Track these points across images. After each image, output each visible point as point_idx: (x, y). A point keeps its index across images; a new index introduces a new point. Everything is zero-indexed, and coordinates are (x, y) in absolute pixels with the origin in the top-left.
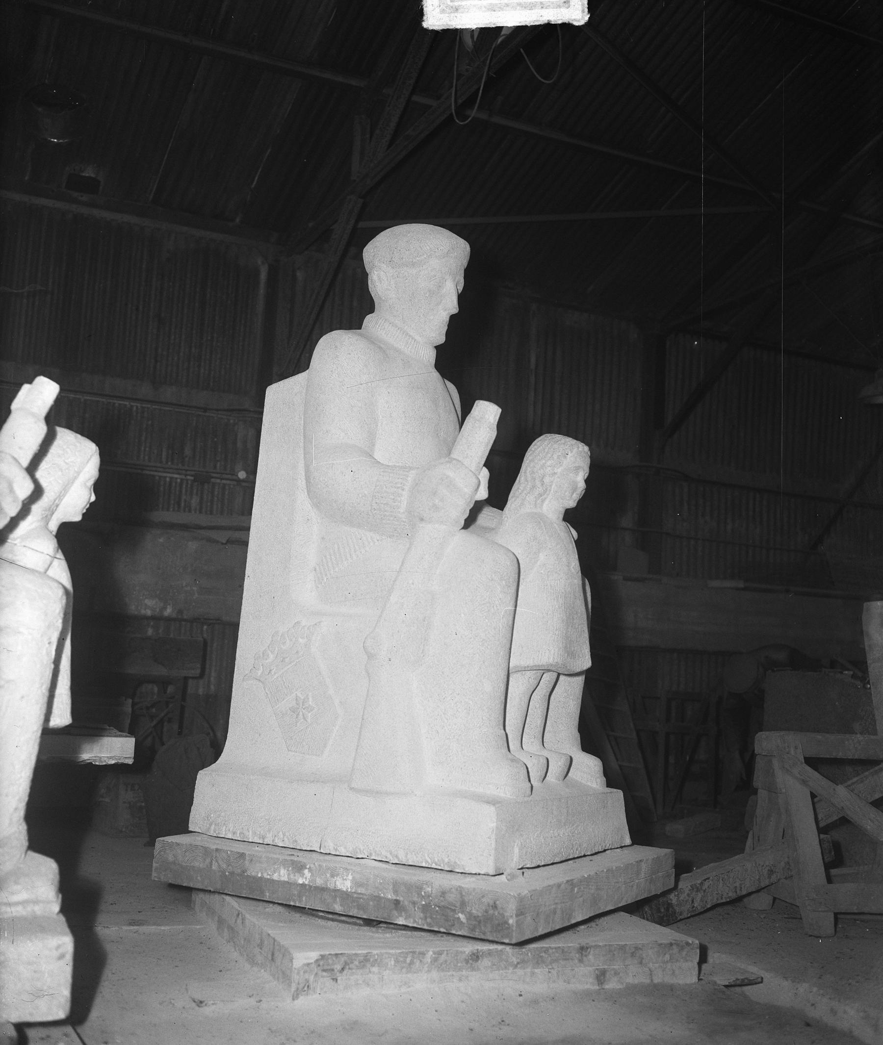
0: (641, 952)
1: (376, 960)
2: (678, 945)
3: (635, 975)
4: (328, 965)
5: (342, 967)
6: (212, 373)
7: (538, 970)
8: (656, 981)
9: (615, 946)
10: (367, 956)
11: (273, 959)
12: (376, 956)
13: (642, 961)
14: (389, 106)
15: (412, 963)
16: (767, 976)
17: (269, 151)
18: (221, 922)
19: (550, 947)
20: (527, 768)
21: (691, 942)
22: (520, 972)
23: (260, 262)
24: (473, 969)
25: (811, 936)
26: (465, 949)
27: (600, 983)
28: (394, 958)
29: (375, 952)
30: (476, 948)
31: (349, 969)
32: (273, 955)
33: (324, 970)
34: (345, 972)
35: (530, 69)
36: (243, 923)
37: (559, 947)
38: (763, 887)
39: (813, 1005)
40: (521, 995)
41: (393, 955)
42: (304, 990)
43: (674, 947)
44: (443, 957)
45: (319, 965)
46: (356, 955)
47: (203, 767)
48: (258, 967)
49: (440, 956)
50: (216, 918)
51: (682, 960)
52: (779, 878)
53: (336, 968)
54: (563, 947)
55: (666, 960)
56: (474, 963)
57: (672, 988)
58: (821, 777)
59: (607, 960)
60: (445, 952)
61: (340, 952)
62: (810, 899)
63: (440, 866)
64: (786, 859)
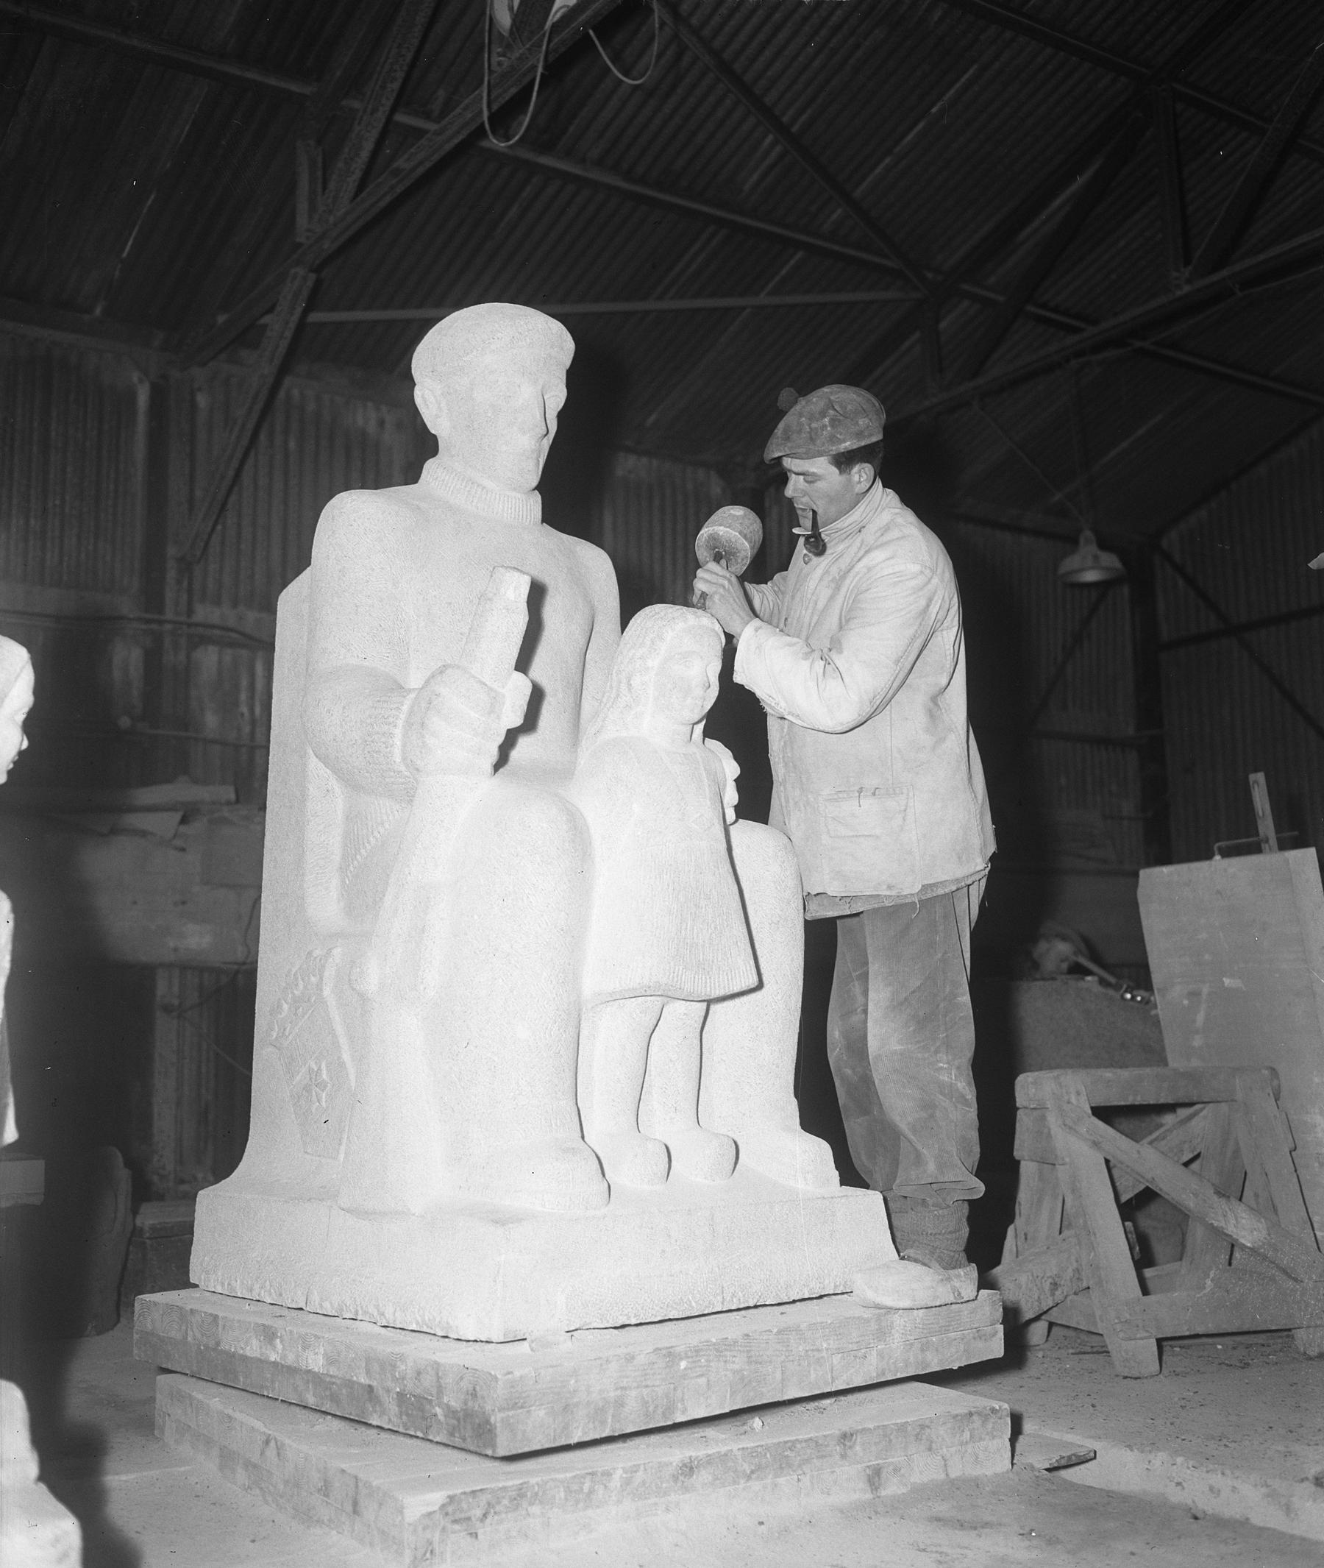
0: (928, 1430)
1: (536, 1494)
2: (979, 1414)
3: (924, 1470)
4: (462, 1511)
5: (484, 1512)
6: (66, 559)
7: (781, 1479)
8: (953, 1476)
9: (893, 1426)
10: (521, 1489)
11: (355, 1512)
12: (536, 1488)
13: (931, 1445)
14: (359, 123)
15: (591, 1492)
16: (1096, 1445)
17: (153, 197)
18: (228, 1458)
19: (797, 1440)
20: (598, 1158)
21: (998, 1408)
22: (756, 1485)
23: (135, 379)
24: (686, 1490)
25: (1125, 1377)
26: (671, 1459)
27: (873, 1487)
28: (564, 1486)
29: (533, 1481)
30: (687, 1455)
31: (495, 1513)
32: (355, 1504)
33: (455, 1521)
34: (488, 1521)
35: (602, 58)
36: (279, 1454)
37: (811, 1439)
38: (1045, 1310)
39: (1178, 1484)
40: (761, 1523)
41: (562, 1482)
42: (425, 1558)
43: (975, 1418)
44: (640, 1476)
45: (447, 1514)
46: (504, 1489)
47: (840, 1174)
48: (321, 1527)
49: (634, 1474)
50: (215, 1452)
51: (987, 1437)
52: (1065, 1293)
53: (475, 1515)
54: (816, 1437)
55: (965, 1440)
56: (686, 1480)
57: (976, 1483)
58: (1118, 1135)
59: (882, 1450)
60: (642, 1468)
61: (479, 1488)
62: (1122, 1322)
63: (432, 1328)
64: (1075, 1265)
